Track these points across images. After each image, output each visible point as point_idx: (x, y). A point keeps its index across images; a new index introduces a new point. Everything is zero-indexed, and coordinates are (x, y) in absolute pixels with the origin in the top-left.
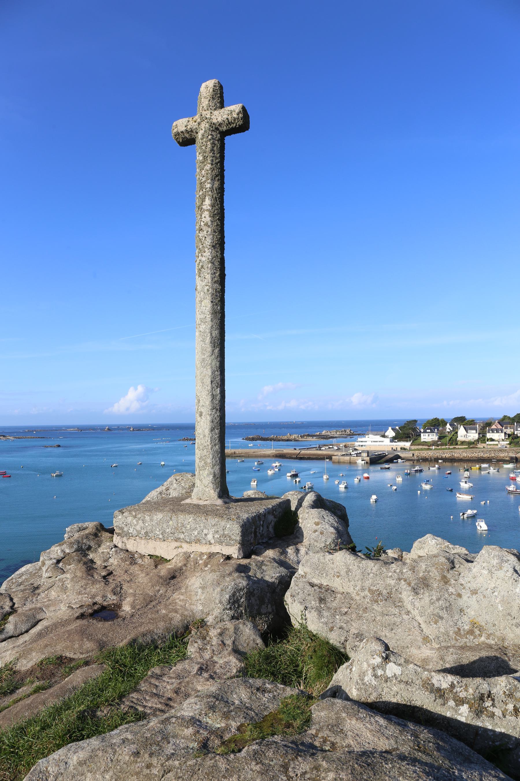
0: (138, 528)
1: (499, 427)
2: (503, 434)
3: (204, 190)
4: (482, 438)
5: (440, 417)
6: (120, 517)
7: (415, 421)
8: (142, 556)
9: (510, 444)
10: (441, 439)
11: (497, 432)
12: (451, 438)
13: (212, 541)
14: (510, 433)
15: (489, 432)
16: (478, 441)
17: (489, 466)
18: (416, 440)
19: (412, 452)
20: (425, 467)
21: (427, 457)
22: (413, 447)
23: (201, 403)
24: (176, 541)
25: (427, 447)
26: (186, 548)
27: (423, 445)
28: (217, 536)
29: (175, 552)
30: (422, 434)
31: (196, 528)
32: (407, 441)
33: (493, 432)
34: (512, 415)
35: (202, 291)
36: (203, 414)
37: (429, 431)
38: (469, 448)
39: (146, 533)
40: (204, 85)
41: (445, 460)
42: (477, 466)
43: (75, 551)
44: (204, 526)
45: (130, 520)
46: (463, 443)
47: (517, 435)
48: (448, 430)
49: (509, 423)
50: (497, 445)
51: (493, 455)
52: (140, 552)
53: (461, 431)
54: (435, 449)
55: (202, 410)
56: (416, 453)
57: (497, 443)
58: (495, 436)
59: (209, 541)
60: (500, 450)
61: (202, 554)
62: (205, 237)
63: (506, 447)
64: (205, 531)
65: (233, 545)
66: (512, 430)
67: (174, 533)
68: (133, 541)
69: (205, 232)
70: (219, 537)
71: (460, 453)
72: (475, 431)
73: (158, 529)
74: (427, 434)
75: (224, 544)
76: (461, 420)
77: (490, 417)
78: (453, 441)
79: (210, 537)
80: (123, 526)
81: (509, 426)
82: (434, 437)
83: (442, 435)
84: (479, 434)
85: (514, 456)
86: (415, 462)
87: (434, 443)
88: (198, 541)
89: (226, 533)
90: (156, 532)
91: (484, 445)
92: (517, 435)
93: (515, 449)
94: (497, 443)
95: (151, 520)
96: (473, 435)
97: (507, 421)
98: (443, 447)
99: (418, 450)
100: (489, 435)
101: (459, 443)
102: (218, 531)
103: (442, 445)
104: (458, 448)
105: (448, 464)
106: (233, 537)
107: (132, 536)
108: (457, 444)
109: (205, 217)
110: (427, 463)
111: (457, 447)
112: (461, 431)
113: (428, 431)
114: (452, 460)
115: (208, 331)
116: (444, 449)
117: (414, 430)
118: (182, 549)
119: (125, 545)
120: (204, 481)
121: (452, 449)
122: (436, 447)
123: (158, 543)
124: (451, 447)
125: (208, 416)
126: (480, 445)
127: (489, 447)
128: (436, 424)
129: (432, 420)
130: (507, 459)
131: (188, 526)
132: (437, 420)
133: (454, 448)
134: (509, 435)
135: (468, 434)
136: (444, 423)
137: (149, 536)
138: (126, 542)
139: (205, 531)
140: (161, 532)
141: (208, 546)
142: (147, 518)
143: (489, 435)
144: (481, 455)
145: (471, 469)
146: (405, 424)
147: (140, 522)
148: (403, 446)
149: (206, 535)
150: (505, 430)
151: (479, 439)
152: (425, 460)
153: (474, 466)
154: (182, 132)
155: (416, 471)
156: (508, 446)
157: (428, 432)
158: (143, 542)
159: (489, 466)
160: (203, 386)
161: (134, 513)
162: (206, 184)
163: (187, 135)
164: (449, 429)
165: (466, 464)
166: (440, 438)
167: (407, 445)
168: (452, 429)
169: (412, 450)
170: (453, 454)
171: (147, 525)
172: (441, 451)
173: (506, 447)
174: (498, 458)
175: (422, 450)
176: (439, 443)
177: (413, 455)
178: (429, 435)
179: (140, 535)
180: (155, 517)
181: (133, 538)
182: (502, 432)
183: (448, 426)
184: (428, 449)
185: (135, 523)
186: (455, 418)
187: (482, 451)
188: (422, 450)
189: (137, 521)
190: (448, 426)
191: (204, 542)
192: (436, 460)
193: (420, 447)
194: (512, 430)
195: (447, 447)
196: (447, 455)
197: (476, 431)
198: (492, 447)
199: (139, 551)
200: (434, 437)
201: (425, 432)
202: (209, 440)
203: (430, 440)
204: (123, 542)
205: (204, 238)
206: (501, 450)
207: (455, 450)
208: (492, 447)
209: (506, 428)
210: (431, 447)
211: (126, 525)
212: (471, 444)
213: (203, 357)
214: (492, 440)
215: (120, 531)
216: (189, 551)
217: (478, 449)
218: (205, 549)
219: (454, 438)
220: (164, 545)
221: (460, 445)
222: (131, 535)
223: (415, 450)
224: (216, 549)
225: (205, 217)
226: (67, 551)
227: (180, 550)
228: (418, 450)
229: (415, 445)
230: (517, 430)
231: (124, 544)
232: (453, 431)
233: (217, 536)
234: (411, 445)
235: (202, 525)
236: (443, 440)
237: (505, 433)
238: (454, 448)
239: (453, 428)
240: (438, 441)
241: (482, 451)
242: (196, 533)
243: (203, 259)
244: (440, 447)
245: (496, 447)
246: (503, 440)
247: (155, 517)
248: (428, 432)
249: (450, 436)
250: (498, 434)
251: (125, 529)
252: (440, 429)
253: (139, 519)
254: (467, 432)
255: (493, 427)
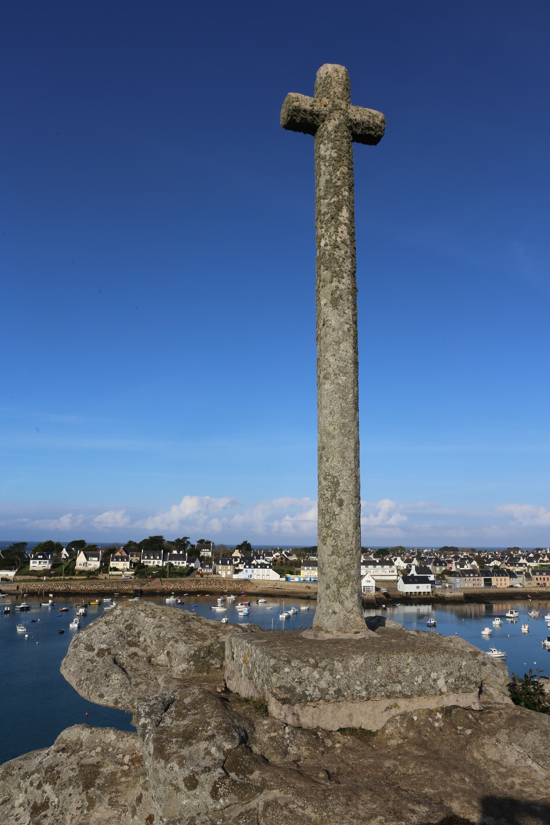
0: (323, 684)
1: (124, 554)
2: (128, 563)
3: (340, 197)
4: (105, 568)
5: (55, 540)
6: (287, 670)
7: (25, 544)
8: (329, 734)
9: (135, 575)
10: (55, 568)
11: (123, 560)
12: (68, 566)
13: (444, 689)
14: (136, 561)
15: (113, 560)
16: (99, 570)
17: (112, 601)
18: (22, 568)
19: (17, 584)
20: (34, 602)
21: (36, 590)
22: (18, 578)
23: (342, 487)
24: (388, 697)
25: (36, 578)
26: (404, 705)
27: (31, 575)
28: (451, 680)
29: (386, 717)
30: (31, 561)
31: (418, 673)
32: (11, 570)
33: (117, 560)
34: (138, 542)
35: (340, 329)
36: (345, 504)
37: (41, 557)
38: (89, 579)
39: (338, 692)
40: (322, 68)
41: (57, 594)
42: (97, 601)
43: (240, 744)
44: (432, 668)
45: (307, 672)
46: (81, 572)
47: (143, 564)
48: (63, 557)
49: (134, 550)
50: (121, 575)
51: (115, 588)
52: (323, 727)
53: (81, 558)
54: (47, 580)
55: (343, 497)
56: (22, 585)
57: (121, 573)
58: (120, 565)
59: (440, 690)
60: (124, 582)
61: (431, 713)
62: (344, 259)
63: (131, 578)
64: (434, 675)
65: (472, 691)
66: (138, 558)
67: (386, 685)
68: (312, 710)
69: (343, 252)
70: (453, 680)
71: (78, 585)
72: (96, 559)
73: (358, 683)
74: (38, 561)
75: (460, 691)
76: (79, 545)
77: (114, 542)
78: (70, 570)
79: (441, 683)
80: (295, 684)
81: (135, 553)
82: (46, 565)
83: (56, 563)
84: (101, 562)
85: (139, 588)
86: (20, 597)
87: (46, 573)
88: (422, 692)
89: (463, 673)
90: (356, 687)
91: (105, 575)
92: (143, 564)
93: (140, 580)
94: (121, 573)
95: (346, 668)
96: (95, 564)
97: (133, 547)
98: (56, 578)
99: (25, 581)
100: (112, 564)
101: (77, 573)
102: (451, 673)
103: (56, 575)
104: (75, 579)
105: (61, 599)
106: (472, 678)
107: (311, 701)
108: (74, 574)
109: (342, 232)
110: (35, 597)
111: (74, 577)
112: (81, 558)
113: (39, 557)
114: (67, 594)
115: (350, 386)
116: (57, 580)
117: (22, 555)
118: (396, 709)
119: (298, 719)
120: (346, 603)
121: (67, 580)
122: (48, 578)
123: (357, 706)
124: (66, 578)
125: (351, 506)
126: (102, 576)
127: (111, 578)
128: (48, 549)
129: (45, 543)
130: (131, 592)
131: (408, 671)
132: (50, 543)
133: (71, 579)
134: (135, 564)
135: (88, 562)
136: (58, 547)
137: (343, 696)
138: (300, 712)
139: (434, 675)
140: (364, 686)
141: (438, 698)
142: (338, 666)
143: (112, 564)
144: (103, 587)
145: (90, 605)
146: (11, 547)
147: (327, 674)
148: (5, 577)
149: (435, 681)
150: (130, 558)
151: (100, 567)
152: (32, 594)
153: (92, 601)
154: (305, 111)
155: (22, 609)
156: (133, 577)
157: (40, 559)
158: (330, 707)
159: (112, 601)
160: (343, 462)
161: (312, 661)
162: (343, 190)
163: (309, 118)
164: (65, 555)
165: (83, 599)
166: (53, 567)
167: (11, 574)
168: (68, 556)
169: (17, 581)
170: (69, 586)
171: (338, 677)
172: (54, 583)
173: (131, 578)
174: (122, 592)
175: (29, 581)
176: (52, 572)
177: (18, 587)
178: (40, 562)
179: (327, 697)
180: (352, 663)
181: (312, 704)
182: (127, 561)
183: (64, 551)
184: (38, 580)
185: (317, 676)
186: (73, 542)
187: (104, 583)
188: (29, 581)
189: (320, 673)
190: (64, 551)
191: (433, 691)
192: (47, 593)
193: (28, 577)
194: (138, 558)
195: (62, 577)
196: (61, 588)
197: (98, 559)
198: (115, 577)
199: (323, 725)
200: (46, 565)
201: (36, 558)
202: (354, 542)
203: (42, 569)
204: (294, 714)
205: (341, 259)
206: (125, 582)
207: (72, 582)
208: (115, 577)
209: (132, 556)
210: (41, 578)
211: (300, 683)
212: (91, 575)
213: (343, 421)
214: (115, 569)
215: (288, 696)
216: (409, 711)
217: (99, 581)
218: (432, 703)
219: (71, 567)
220: (367, 707)
221: (78, 575)
222: (309, 698)
223: (20, 581)
224: (450, 700)
225: (342, 232)
226: (228, 746)
227: (393, 712)
228: (25, 581)
229: (20, 575)
230: (144, 559)
231: (296, 717)
232: (70, 557)
233: (451, 680)
234: (16, 575)
235: (428, 666)
236: (57, 569)
237: (131, 562)
238: (71, 579)
239: (70, 554)
240: (50, 570)
241: (104, 583)
242: (420, 680)
243: (342, 287)
244: (53, 578)
245: (120, 578)
246: (128, 570)
247: (352, 663)
248: (40, 559)
249: (66, 564)
250: (123, 563)
251: (299, 690)
252: (54, 554)
253: (324, 669)
254: (87, 559)
255: (118, 554)
